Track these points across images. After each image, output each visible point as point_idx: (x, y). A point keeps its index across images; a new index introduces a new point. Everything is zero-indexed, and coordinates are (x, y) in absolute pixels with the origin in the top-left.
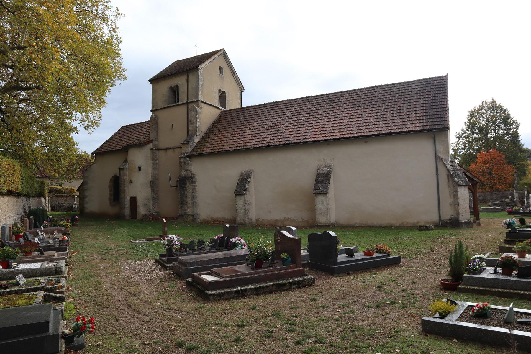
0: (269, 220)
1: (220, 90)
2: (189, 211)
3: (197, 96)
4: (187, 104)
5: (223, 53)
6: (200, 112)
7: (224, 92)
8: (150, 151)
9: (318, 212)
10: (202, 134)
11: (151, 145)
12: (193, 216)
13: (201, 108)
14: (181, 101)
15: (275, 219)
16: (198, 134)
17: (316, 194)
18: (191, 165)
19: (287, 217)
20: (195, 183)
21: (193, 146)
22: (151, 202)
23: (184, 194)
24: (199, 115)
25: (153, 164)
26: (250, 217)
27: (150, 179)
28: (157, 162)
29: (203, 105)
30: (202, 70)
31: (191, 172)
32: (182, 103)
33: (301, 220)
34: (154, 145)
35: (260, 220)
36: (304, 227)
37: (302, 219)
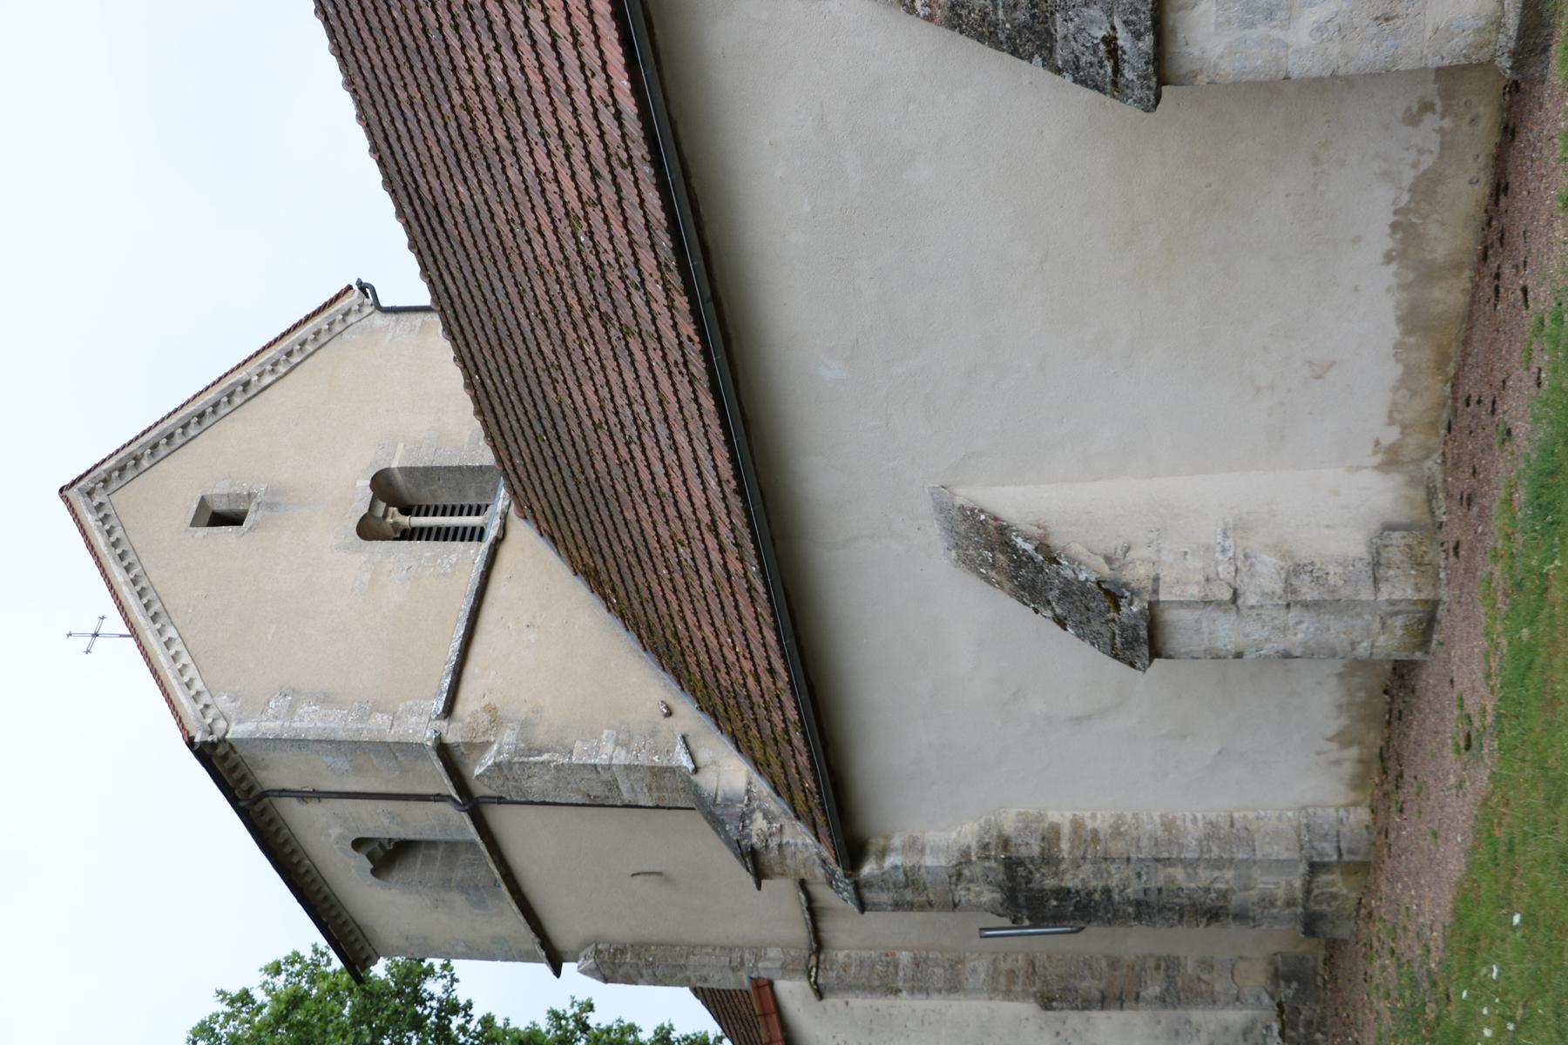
0: (1394, 372)
1: (368, 529)
2: (1284, 884)
3: (404, 750)
4: (473, 805)
5: (95, 494)
6: (525, 725)
7: (383, 485)
8: (829, 1001)
9: (1367, 51)
10: (688, 715)
11: (792, 992)
12: (1315, 868)
13: (495, 718)
14: (463, 829)
15: (1394, 331)
16: (684, 760)
17: (1162, 70)
18: (914, 846)
19: (1380, 239)
20: (1051, 836)
21: (776, 805)
22: (1197, 1015)
23: (1138, 904)
24: (541, 736)
25: (920, 987)
26: (1353, 545)
27: (1026, 1008)
28: (905, 957)
29: (469, 703)
30: (222, 702)
31: (965, 859)
32: (472, 829)
33: (1431, 121)
34: (787, 970)
35: (1391, 435)
36: (1509, 131)
37: (1413, 119)
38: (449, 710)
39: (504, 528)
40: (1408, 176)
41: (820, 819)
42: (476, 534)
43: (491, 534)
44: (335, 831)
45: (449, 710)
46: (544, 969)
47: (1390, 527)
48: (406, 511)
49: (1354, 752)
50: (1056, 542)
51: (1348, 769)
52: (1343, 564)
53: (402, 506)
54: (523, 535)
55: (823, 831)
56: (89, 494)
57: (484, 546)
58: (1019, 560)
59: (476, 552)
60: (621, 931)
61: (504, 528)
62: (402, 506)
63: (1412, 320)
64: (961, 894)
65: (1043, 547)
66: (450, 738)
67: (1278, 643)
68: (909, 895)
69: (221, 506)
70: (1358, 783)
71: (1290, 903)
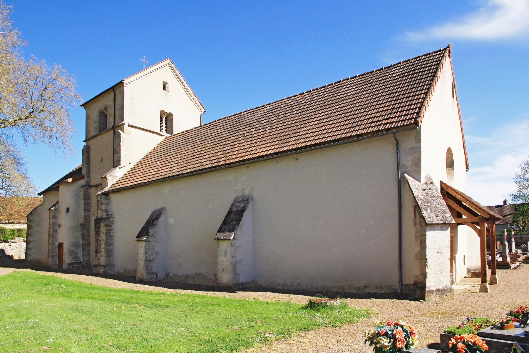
15: (186, 274)
35: (171, 275)
38: (129, 126)
39: (162, 135)
40: (207, 275)
41: (112, 189)
42: (161, 130)
43: (161, 133)
44: (108, 104)
45: (129, 126)
46: (84, 139)
47: (157, 275)
48: (166, 118)
49: (123, 272)
50: (155, 226)
51: (120, 271)
52: (151, 268)
53: (167, 119)
54: (162, 138)
55: (110, 189)
56: (169, 64)
57: (159, 132)
58: (153, 221)
59: (158, 131)
60: (92, 153)
61: (162, 135)
62: (167, 119)
63: (187, 276)
64: (100, 211)
65: (155, 224)
66: (125, 126)
67: (139, 259)
68: (100, 203)
69: (166, 86)
70: (118, 273)
71: (99, 263)
